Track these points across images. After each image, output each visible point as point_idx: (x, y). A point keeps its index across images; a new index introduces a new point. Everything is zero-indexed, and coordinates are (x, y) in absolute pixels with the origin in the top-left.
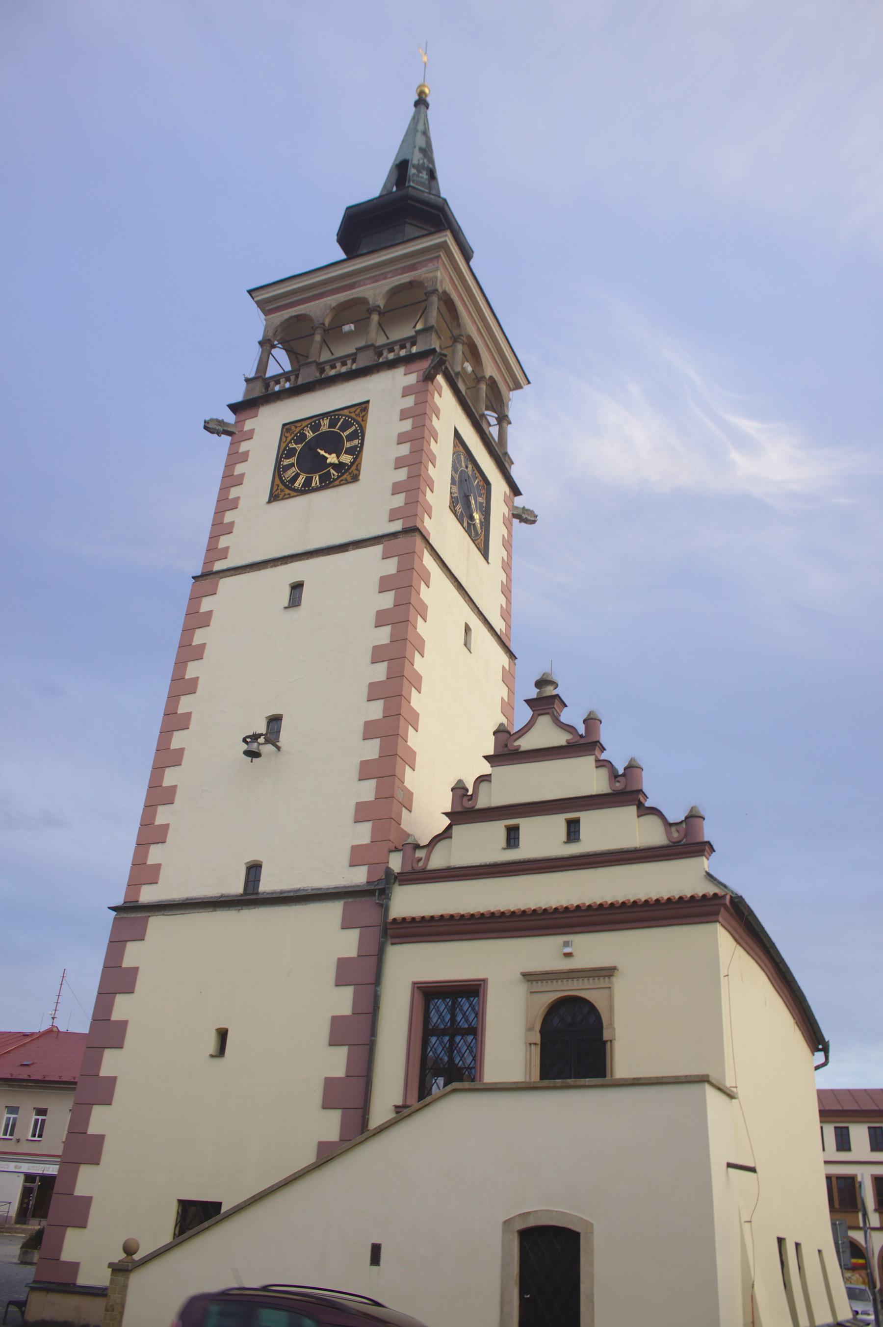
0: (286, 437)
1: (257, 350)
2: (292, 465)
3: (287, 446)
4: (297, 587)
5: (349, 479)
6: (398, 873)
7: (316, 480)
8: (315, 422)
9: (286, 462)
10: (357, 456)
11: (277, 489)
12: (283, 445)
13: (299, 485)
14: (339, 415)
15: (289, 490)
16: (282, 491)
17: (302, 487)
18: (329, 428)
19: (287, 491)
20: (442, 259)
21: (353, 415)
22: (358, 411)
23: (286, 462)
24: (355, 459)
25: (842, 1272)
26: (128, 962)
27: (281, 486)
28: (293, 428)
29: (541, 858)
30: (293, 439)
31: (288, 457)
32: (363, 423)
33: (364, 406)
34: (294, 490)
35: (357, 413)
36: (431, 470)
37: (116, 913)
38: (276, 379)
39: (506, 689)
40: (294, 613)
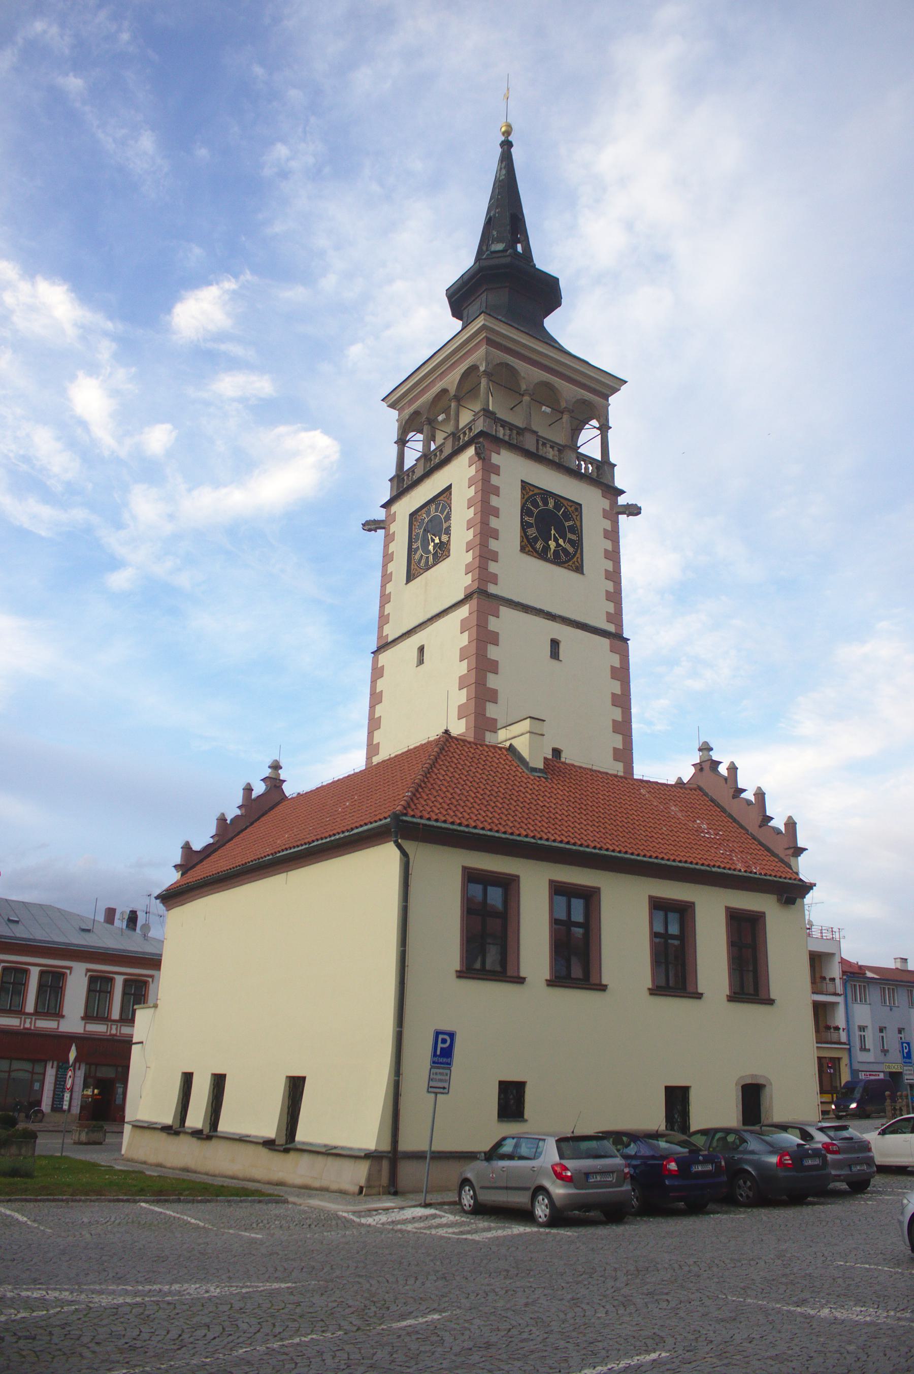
0: (571, 506)
3: (564, 505)
5: (523, 544)
7: (539, 545)
8: (577, 530)
10: (539, 555)
11: (530, 490)
12: (565, 503)
13: (907, 1079)
14: (578, 547)
15: (570, 561)
16: (574, 563)
18: (569, 538)
19: (526, 497)
21: (575, 559)
22: (578, 564)
24: (537, 552)
27: (531, 493)
28: (577, 514)
29: (206, 889)
30: (568, 511)
32: (566, 565)
34: (527, 501)
35: (576, 563)
37: (706, 1137)
38: (412, 469)
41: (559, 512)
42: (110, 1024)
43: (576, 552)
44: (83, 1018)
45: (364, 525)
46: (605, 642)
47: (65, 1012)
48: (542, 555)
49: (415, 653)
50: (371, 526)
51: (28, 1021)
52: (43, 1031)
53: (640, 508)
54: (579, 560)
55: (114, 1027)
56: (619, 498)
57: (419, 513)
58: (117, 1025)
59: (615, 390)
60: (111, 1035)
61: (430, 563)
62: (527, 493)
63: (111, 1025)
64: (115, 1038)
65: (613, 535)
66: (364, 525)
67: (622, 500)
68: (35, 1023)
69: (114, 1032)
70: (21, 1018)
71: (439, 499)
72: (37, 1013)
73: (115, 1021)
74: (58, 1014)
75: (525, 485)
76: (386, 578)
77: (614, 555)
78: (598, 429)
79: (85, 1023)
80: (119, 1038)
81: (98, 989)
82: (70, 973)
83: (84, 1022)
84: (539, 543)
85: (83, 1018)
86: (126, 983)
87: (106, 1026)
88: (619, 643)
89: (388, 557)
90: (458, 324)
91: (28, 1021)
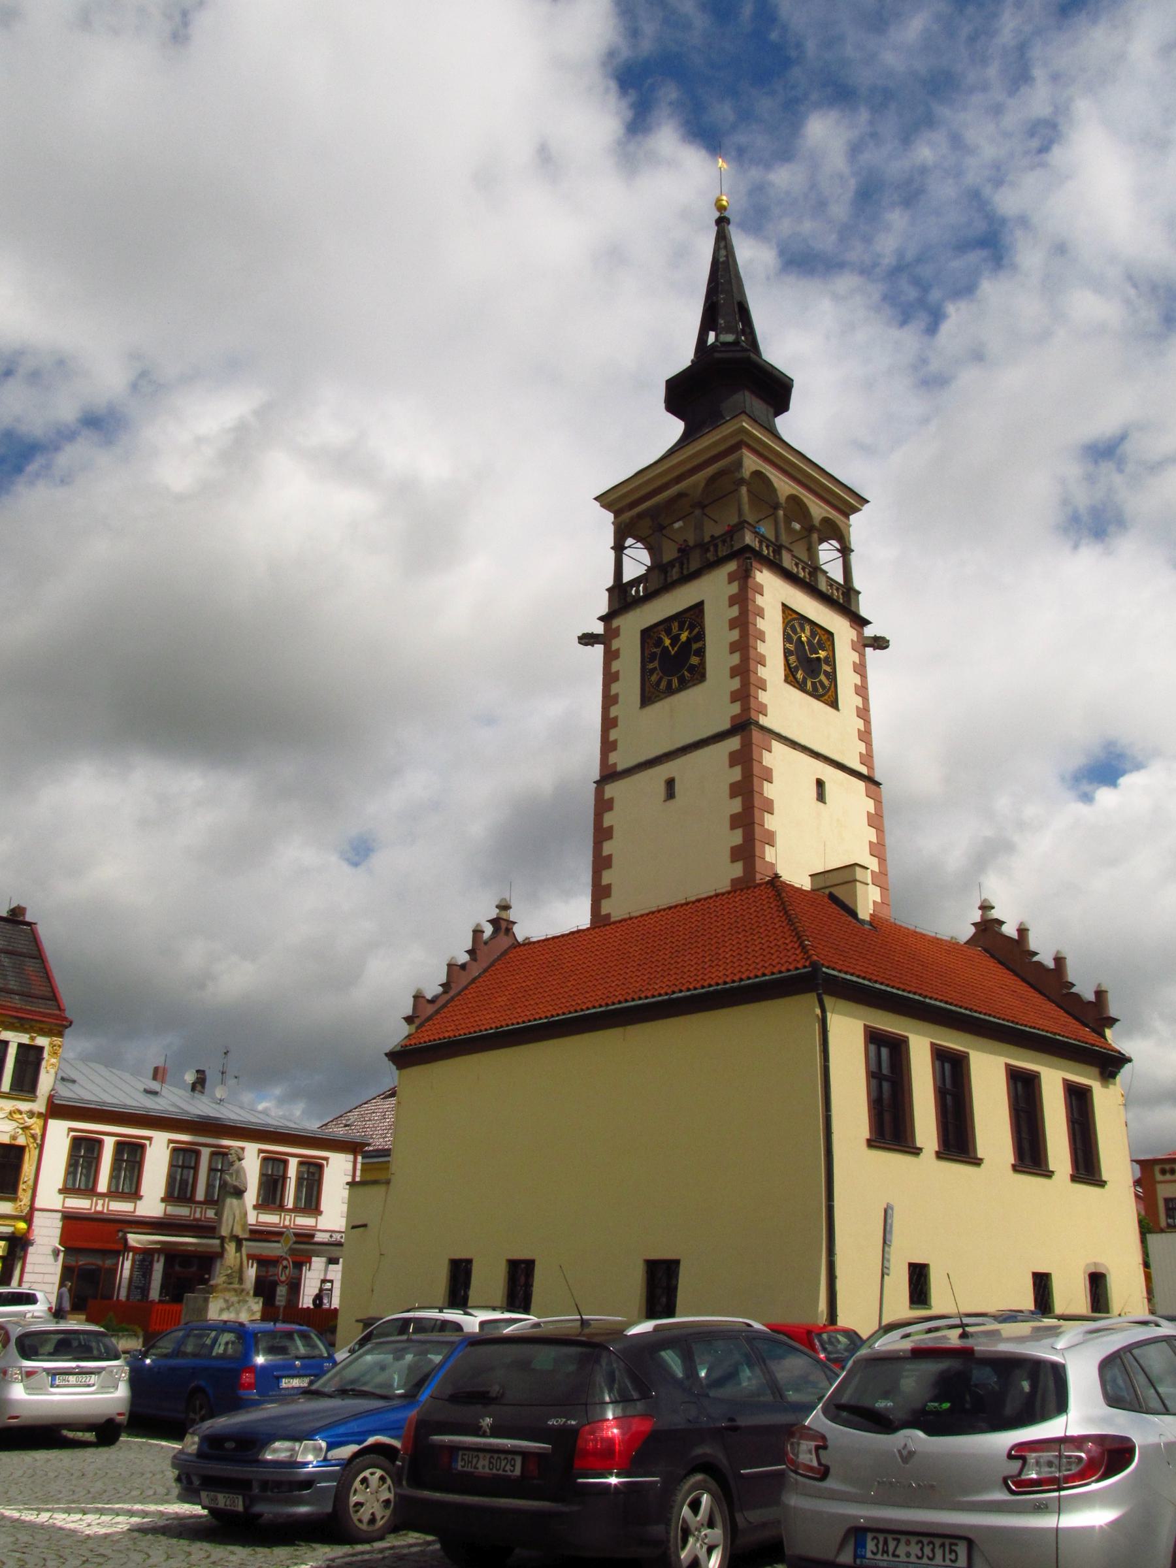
1: (612, 554)
2: (655, 669)
4: (670, 783)
6: (775, 881)
9: (651, 666)
17: (671, 626)
19: (786, 621)
20: (593, 1320)
21: (830, 693)
23: (651, 666)
24: (798, 682)
25: (499, 1404)
26: (606, 824)
31: (651, 661)
33: (699, 607)
36: (760, 600)
38: (635, 582)
39: (857, 654)
40: (671, 803)
41: (814, 639)
42: (193, 1206)
43: (831, 685)
44: (61, 1191)
45: (580, 638)
46: (861, 785)
47: (323, 1207)
48: (801, 687)
49: (661, 789)
50: (587, 639)
51: (198, 1210)
52: (181, 1220)
53: (888, 641)
54: (833, 694)
55: (100, 1202)
56: (865, 629)
57: (655, 630)
58: (202, 1208)
59: (855, 510)
60: (195, 1220)
61: (674, 687)
62: (787, 617)
63: (195, 1207)
64: (200, 1223)
65: (860, 669)
66: (580, 638)
67: (869, 631)
68: (205, 1213)
69: (198, 1215)
70: (191, 1207)
71: (684, 616)
72: (296, 1210)
73: (200, 1203)
74: (135, 1195)
75: (786, 608)
76: (609, 700)
77: (862, 690)
78: (838, 550)
79: (65, 1197)
80: (205, 1223)
81: (220, 1168)
82: (150, 1144)
83: (62, 1196)
84: (800, 672)
85: (61, 1191)
86: (120, 1147)
87: (278, 1217)
88: (873, 787)
89: (610, 677)
90: (676, 427)
91: (198, 1210)
